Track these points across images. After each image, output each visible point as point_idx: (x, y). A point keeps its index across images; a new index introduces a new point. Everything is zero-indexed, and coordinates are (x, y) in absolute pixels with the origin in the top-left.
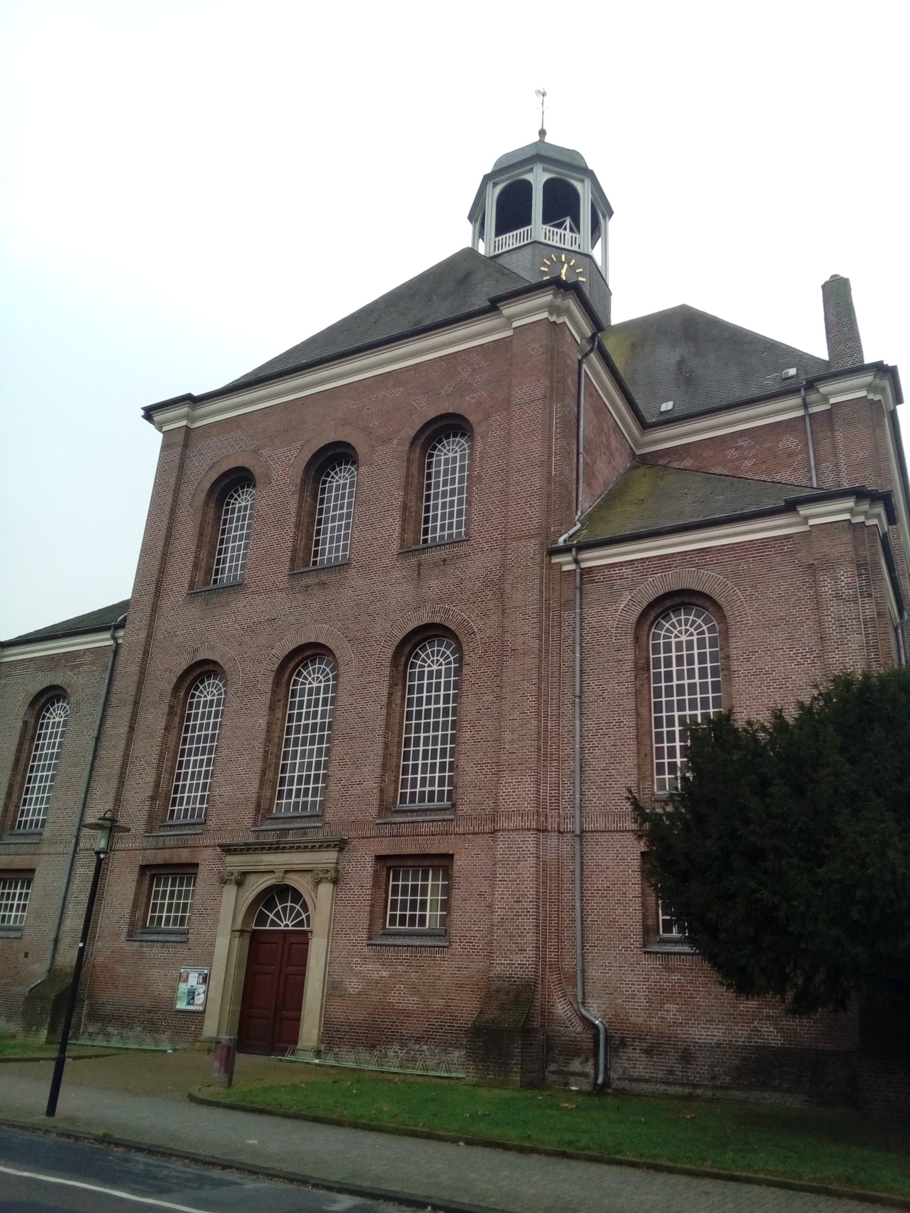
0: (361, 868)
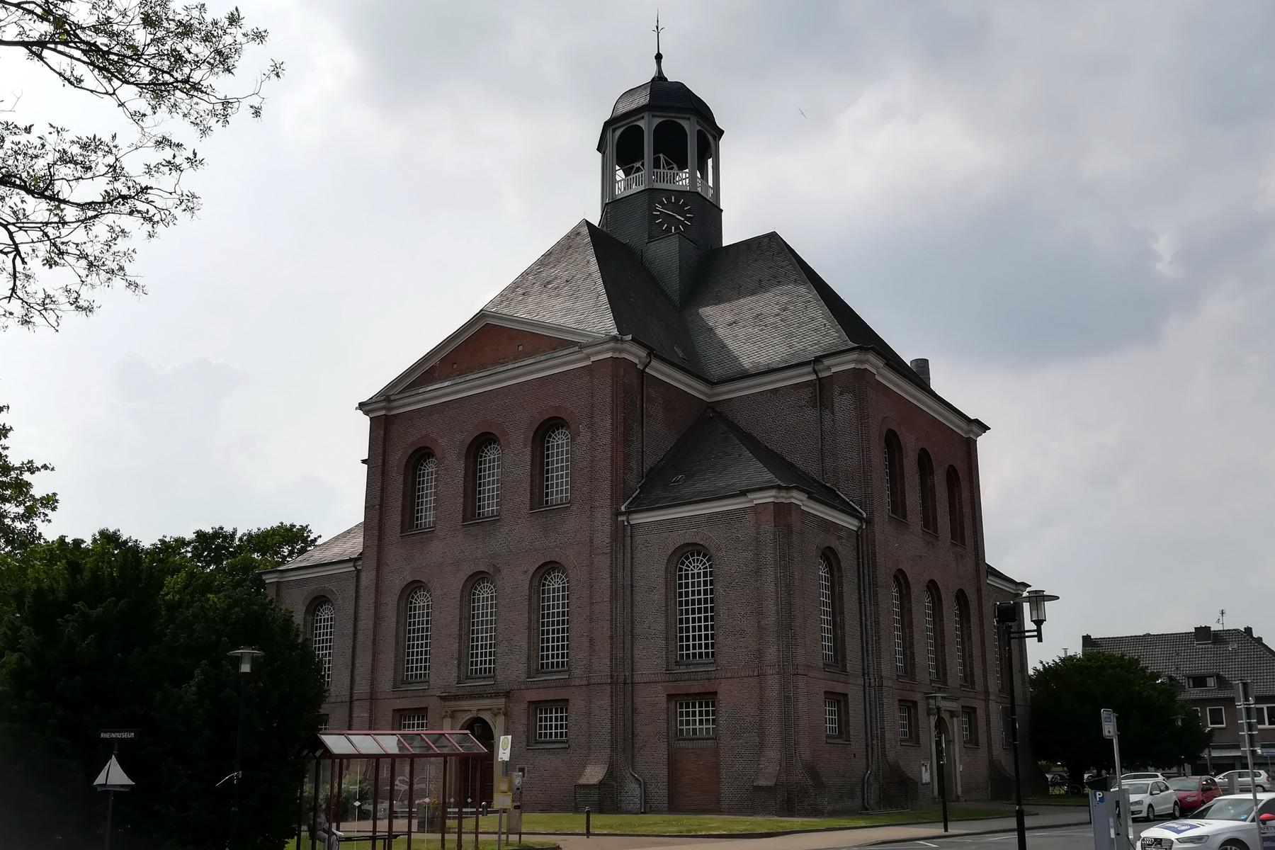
0: (519, 710)
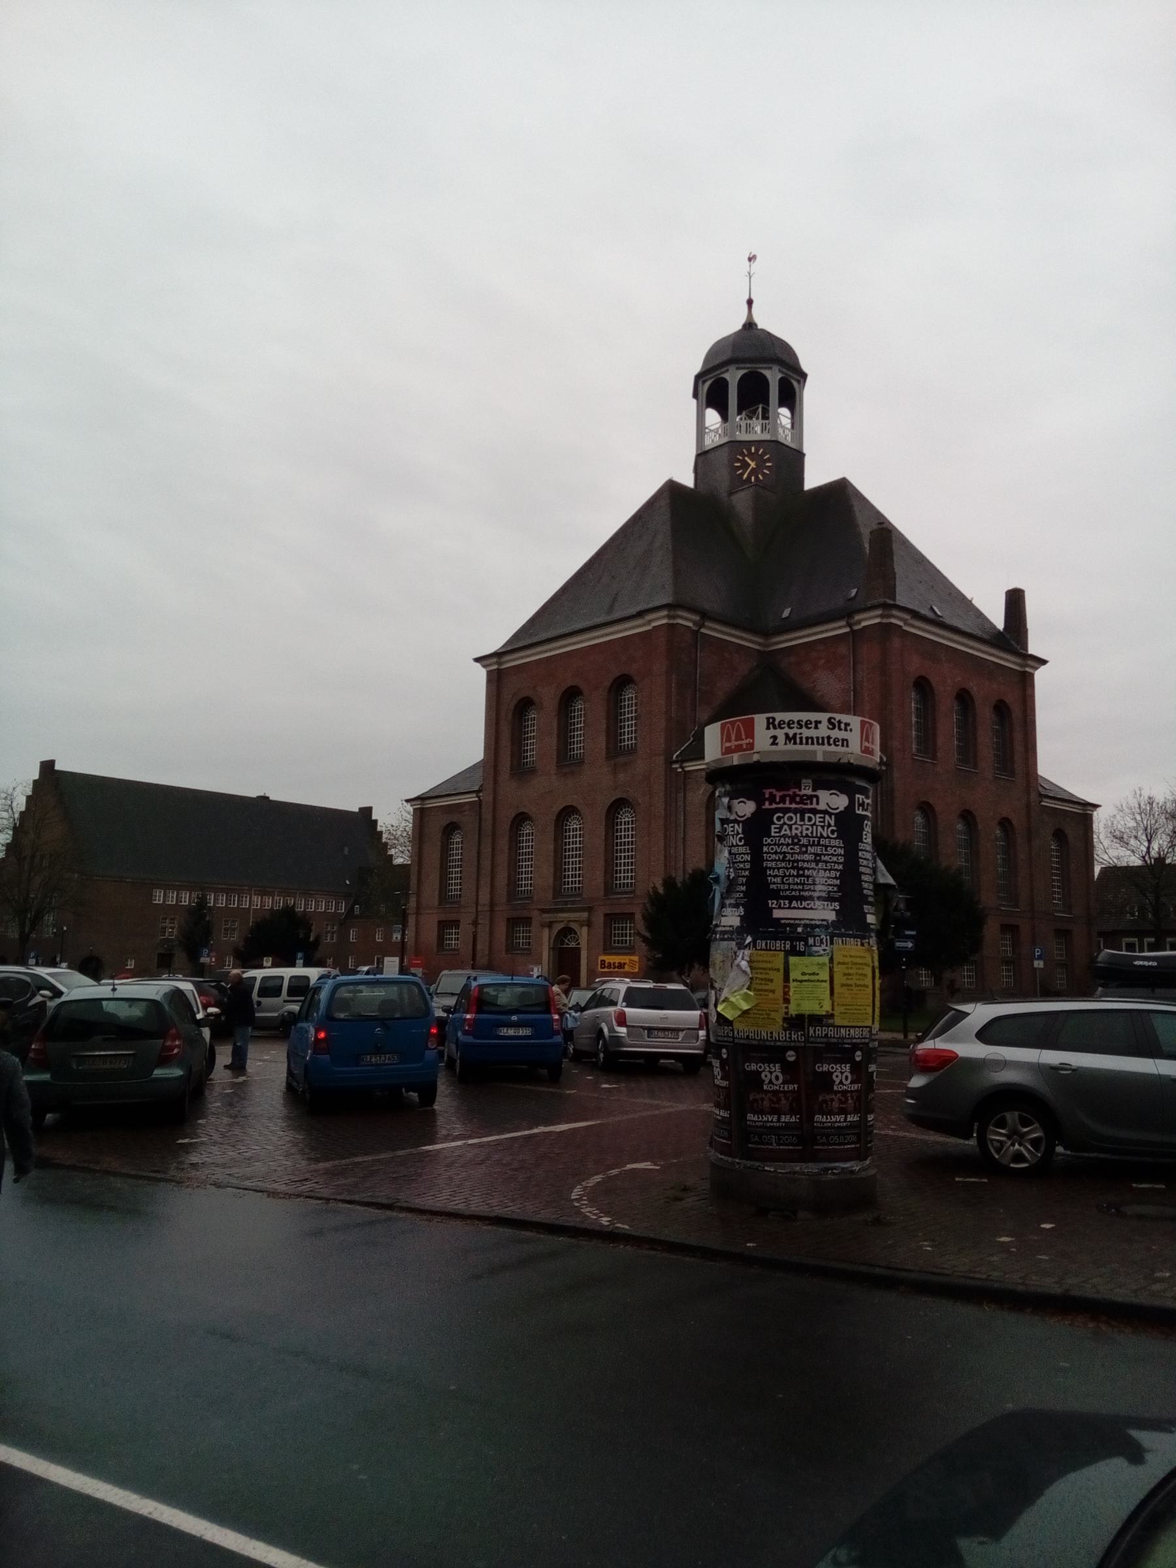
0: (599, 920)
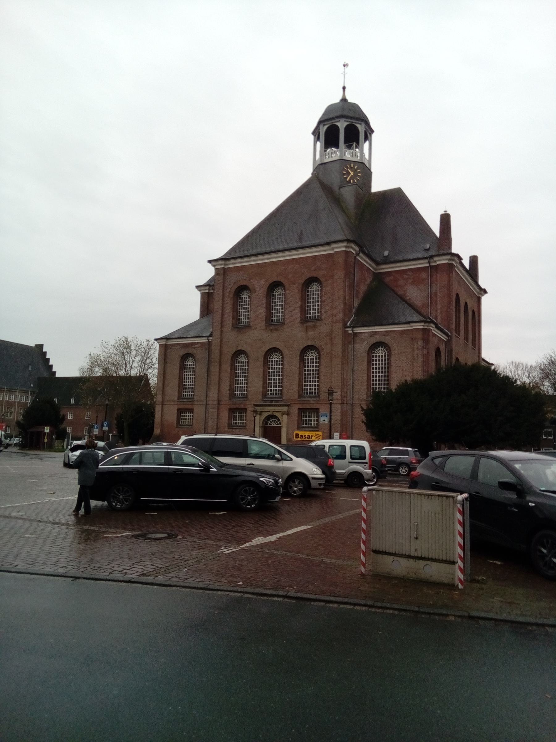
0: (294, 411)
